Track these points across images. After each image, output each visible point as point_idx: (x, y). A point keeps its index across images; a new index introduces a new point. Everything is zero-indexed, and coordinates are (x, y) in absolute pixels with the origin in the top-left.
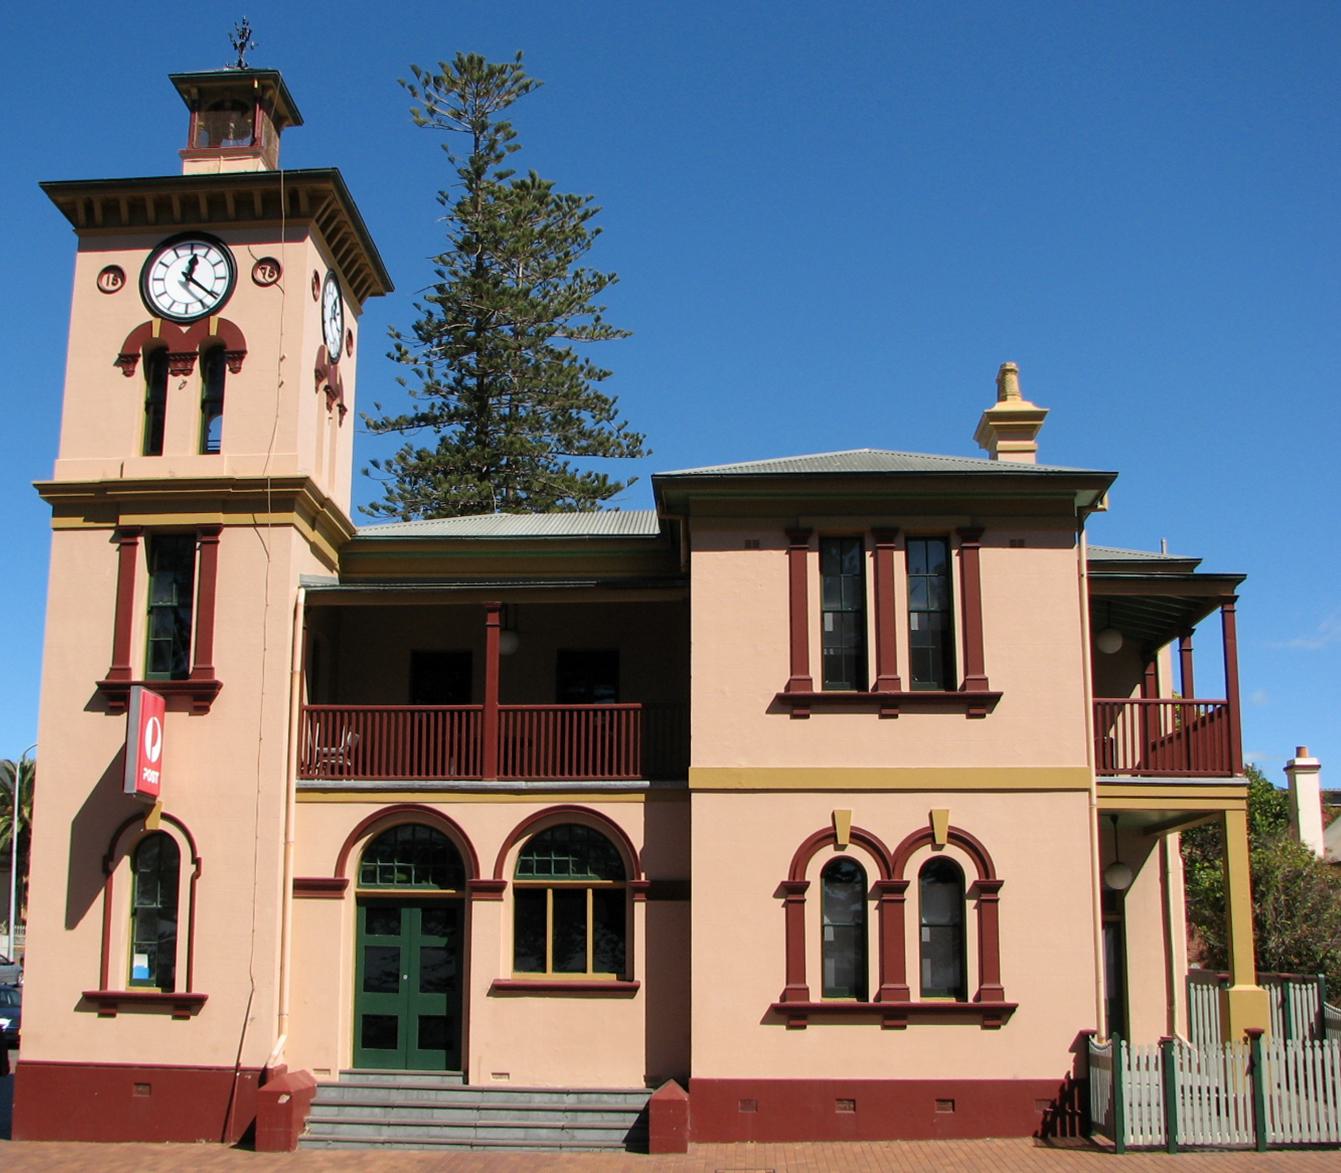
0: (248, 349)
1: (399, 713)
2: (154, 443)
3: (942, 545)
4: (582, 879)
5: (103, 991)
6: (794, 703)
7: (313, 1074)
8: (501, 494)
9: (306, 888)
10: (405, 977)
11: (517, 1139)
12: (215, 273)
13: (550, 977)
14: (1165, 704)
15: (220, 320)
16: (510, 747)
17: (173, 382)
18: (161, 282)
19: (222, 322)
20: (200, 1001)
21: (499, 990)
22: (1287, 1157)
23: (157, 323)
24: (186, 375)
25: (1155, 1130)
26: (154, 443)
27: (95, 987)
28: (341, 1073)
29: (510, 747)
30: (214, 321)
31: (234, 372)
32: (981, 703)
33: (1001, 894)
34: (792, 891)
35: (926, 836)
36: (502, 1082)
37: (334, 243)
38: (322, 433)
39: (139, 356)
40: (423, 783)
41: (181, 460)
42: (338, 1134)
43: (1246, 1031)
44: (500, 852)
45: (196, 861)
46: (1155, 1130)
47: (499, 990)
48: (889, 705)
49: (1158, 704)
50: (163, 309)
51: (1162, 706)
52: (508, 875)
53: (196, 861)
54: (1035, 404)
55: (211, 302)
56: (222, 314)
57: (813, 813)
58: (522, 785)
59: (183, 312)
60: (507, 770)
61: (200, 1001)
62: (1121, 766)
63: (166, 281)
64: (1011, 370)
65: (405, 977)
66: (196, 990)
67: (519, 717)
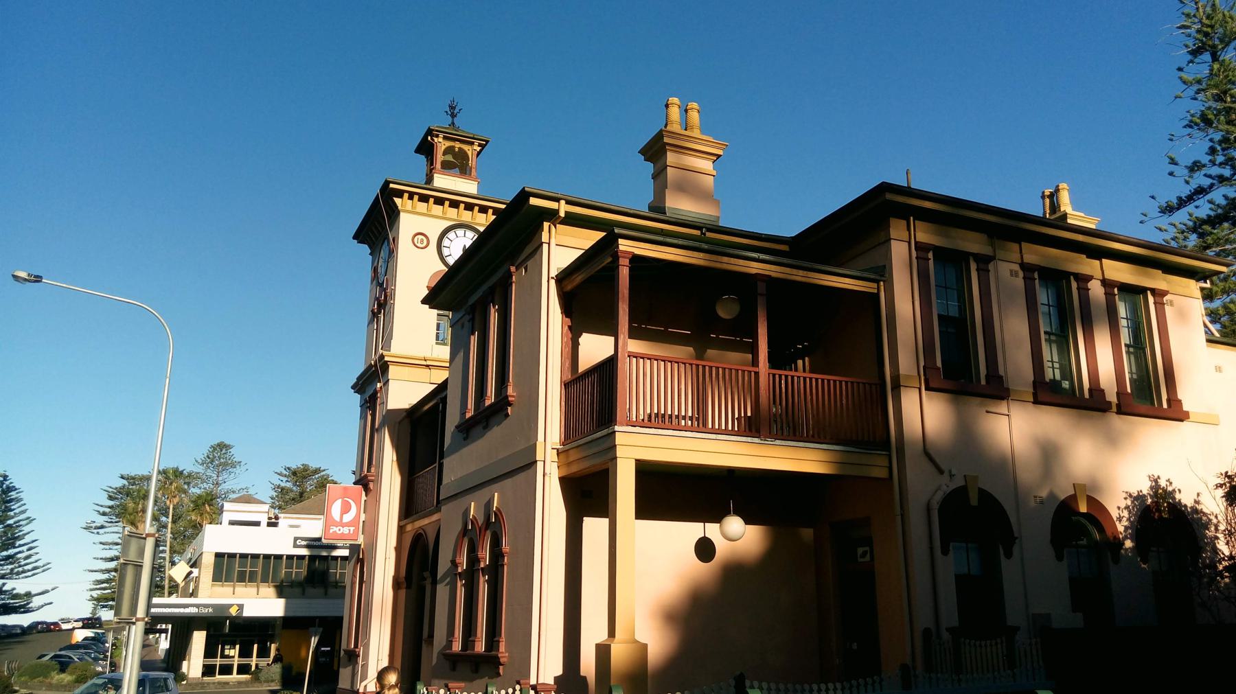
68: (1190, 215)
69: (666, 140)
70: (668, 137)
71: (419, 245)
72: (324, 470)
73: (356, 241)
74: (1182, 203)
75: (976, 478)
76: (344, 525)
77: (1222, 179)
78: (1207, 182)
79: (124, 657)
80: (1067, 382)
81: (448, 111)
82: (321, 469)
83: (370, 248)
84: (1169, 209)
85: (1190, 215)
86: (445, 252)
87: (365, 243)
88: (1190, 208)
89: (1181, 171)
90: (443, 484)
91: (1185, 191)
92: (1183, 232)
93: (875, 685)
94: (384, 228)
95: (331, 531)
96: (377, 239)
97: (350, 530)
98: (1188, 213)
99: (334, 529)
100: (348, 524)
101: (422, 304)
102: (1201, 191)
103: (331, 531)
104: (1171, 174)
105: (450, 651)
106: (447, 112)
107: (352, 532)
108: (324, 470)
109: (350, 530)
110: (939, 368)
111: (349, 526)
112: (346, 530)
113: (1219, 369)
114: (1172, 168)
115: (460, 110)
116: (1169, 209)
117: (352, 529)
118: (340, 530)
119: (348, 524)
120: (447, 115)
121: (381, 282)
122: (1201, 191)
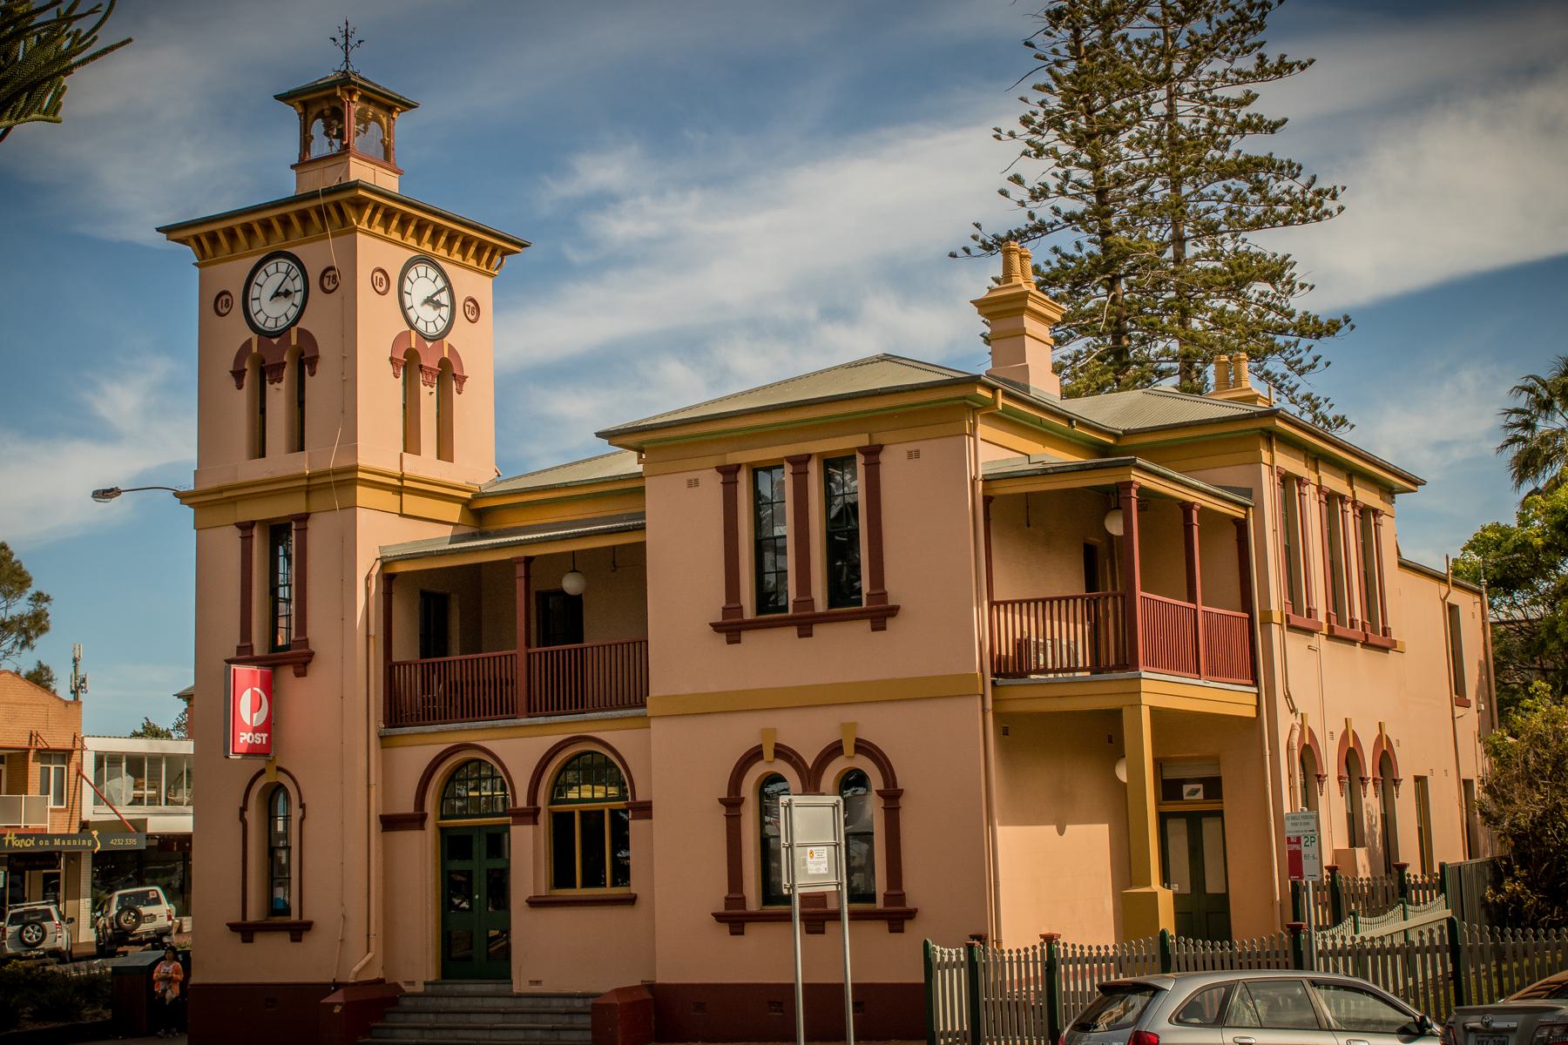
0: (320, 354)
4: (583, 807)
6: (731, 628)
7: (403, 987)
8: (1140, 351)
9: (391, 823)
10: (477, 897)
11: (518, 1040)
13: (579, 892)
15: (298, 328)
16: (561, 679)
17: (270, 388)
19: (300, 331)
20: (308, 926)
21: (535, 903)
23: (255, 337)
24: (279, 382)
26: (259, 450)
27: (237, 919)
28: (426, 984)
29: (561, 679)
30: (294, 330)
31: (459, 393)
32: (882, 615)
33: (901, 801)
34: (732, 804)
35: (834, 750)
36: (536, 989)
39: (245, 370)
40: (472, 724)
41: (280, 462)
42: (394, 1038)
43: (1042, 936)
44: (868, 742)
45: (302, 806)
47: (535, 903)
48: (805, 624)
50: (258, 324)
52: (542, 801)
53: (302, 806)
56: (300, 325)
57: (743, 733)
58: (541, 720)
59: (273, 326)
60: (531, 711)
61: (308, 926)
64: (1015, 250)
65: (477, 897)
66: (306, 918)
69: (1030, 304)
70: (1032, 300)
97: (262, 738)
109: (262, 738)
117: (265, 735)
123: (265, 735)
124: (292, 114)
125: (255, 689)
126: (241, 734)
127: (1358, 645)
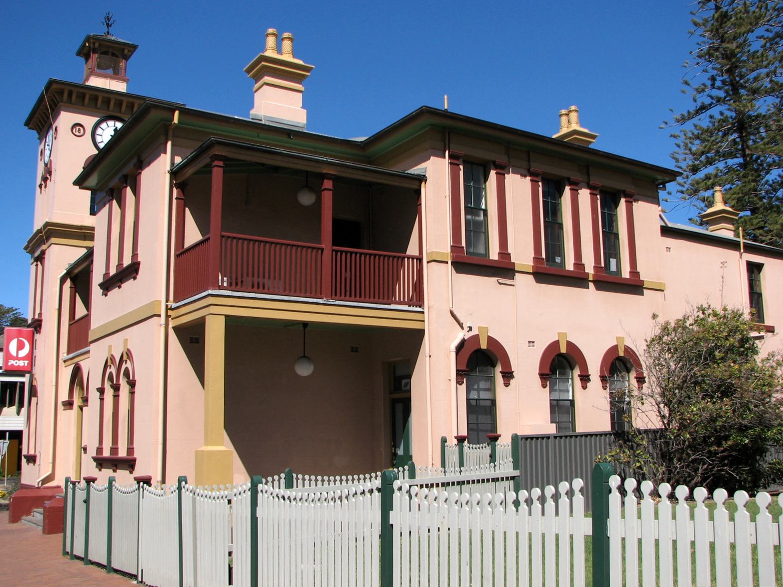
1: (68, 407)
2: (111, 481)
3: (481, 169)
5: (114, 457)
12: (103, 132)
14: (408, 258)
18: (107, 126)
22: (60, 420)
25: (508, 456)
37: (606, 216)
38: (196, 543)
46: (508, 456)
49: (404, 258)
51: (406, 259)
54: (304, 62)
55: (98, 554)
62: (570, 266)
63: (105, 131)
67: (363, 258)
68: (695, 126)
71: (77, 134)
72: (16, 309)
73: (27, 127)
74: (690, 116)
75: (487, 329)
76: (20, 359)
77: (719, 100)
78: (708, 101)
79: (326, 526)
80: (559, 258)
81: (104, 21)
82: (14, 308)
83: (39, 133)
84: (683, 120)
85: (695, 126)
86: (98, 139)
87: (34, 129)
88: (695, 120)
89: (691, 92)
90: (91, 329)
91: (692, 108)
92: (690, 138)
93: (405, 471)
94: (48, 118)
95: (10, 364)
96: (43, 126)
97: (24, 363)
98: (694, 124)
99: (11, 362)
100: (23, 359)
101: (74, 185)
102: (703, 108)
103: (10, 364)
104: (683, 92)
105: (116, 457)
106: (102, 22)
107: (26, 365)
108: (16, 309)
109: (24, 363)
110: (463, 247)
111: (24, 360)
112: (21, 363)
113: (668, 249)
114: (685, 87)
115: (114, 21)
116: (683, 120)
117: (26, 362)
118: (16, 363)
119: (23, 359)
120: (104, 24)
121: (46, 163)
122: (703, 108)
123: (26, 362)
124: (646, 275)
125: (20, 339)
126: (10, 361)
127: (591, 285)
